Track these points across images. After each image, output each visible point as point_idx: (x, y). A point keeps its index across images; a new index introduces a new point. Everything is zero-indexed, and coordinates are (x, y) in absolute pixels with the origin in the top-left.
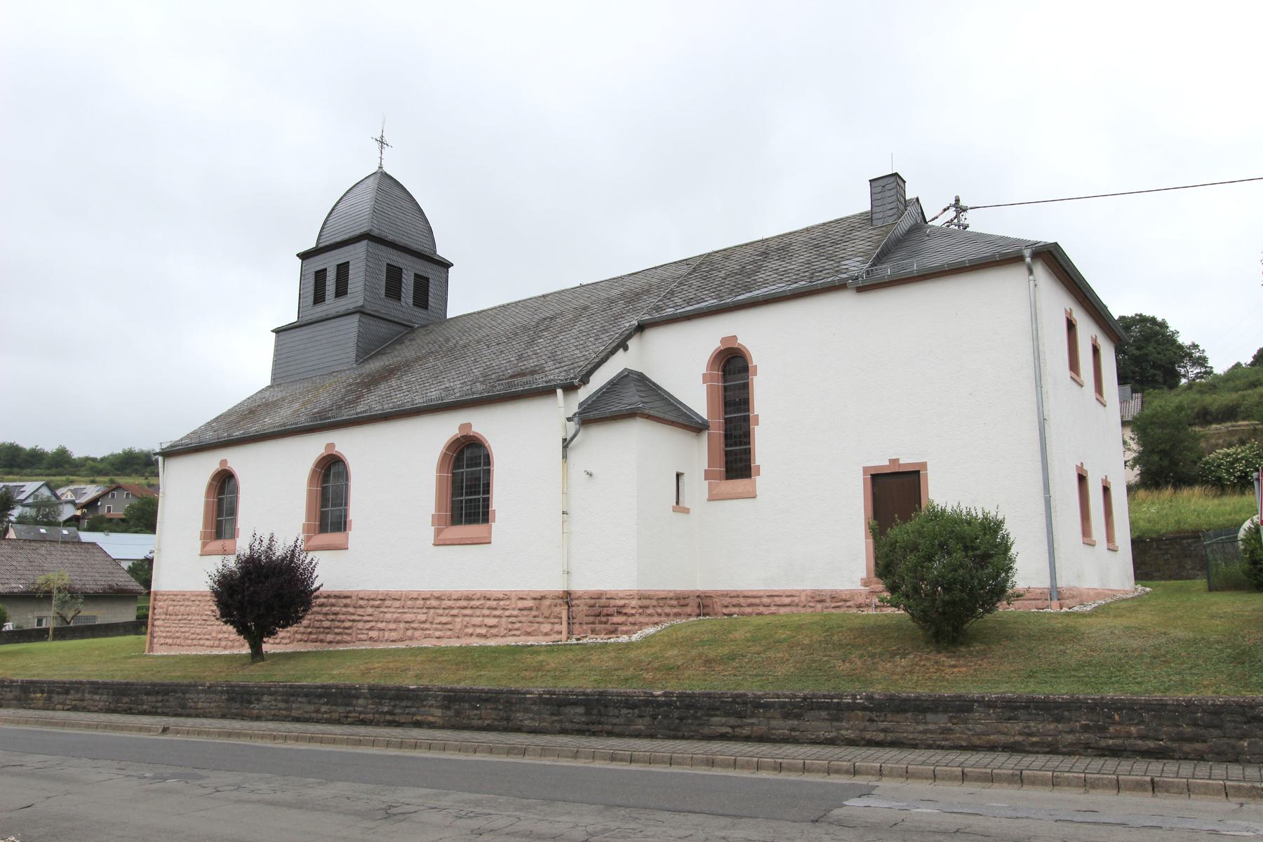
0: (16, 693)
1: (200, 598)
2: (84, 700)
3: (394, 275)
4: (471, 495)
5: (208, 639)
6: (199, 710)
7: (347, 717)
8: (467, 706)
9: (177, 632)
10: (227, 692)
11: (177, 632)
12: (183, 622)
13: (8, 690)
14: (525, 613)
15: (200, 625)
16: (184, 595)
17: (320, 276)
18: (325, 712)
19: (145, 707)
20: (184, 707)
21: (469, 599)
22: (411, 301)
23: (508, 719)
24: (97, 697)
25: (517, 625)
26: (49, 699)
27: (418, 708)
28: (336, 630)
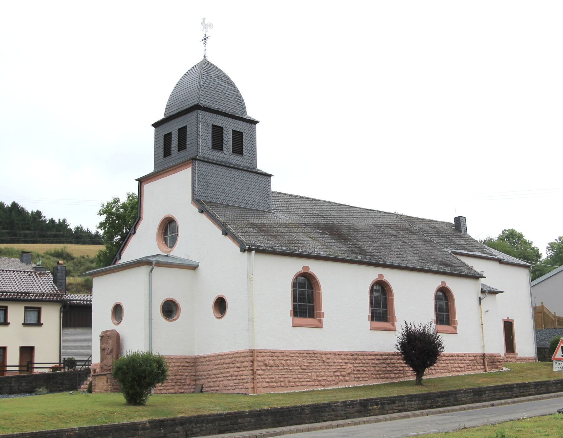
0: (357, 408)
2: (404, 406)
4: (301, 302)
6: (463, 402)
7: (512, 396)
8: (539, 387)
10: (473, 392)
11: (280, 378)
13: (351, 407)
14: (471, 362)
16: (283, 353)
17: (167, 137)
18: (507, 395)
19: (439, 404)
20: (456, 401)
21: (452, 356)
23: (548, 389)
24: (412, 403)
25: (470, 367)
26: (383, 408)
27: (529, 389)
28: (395, 372)
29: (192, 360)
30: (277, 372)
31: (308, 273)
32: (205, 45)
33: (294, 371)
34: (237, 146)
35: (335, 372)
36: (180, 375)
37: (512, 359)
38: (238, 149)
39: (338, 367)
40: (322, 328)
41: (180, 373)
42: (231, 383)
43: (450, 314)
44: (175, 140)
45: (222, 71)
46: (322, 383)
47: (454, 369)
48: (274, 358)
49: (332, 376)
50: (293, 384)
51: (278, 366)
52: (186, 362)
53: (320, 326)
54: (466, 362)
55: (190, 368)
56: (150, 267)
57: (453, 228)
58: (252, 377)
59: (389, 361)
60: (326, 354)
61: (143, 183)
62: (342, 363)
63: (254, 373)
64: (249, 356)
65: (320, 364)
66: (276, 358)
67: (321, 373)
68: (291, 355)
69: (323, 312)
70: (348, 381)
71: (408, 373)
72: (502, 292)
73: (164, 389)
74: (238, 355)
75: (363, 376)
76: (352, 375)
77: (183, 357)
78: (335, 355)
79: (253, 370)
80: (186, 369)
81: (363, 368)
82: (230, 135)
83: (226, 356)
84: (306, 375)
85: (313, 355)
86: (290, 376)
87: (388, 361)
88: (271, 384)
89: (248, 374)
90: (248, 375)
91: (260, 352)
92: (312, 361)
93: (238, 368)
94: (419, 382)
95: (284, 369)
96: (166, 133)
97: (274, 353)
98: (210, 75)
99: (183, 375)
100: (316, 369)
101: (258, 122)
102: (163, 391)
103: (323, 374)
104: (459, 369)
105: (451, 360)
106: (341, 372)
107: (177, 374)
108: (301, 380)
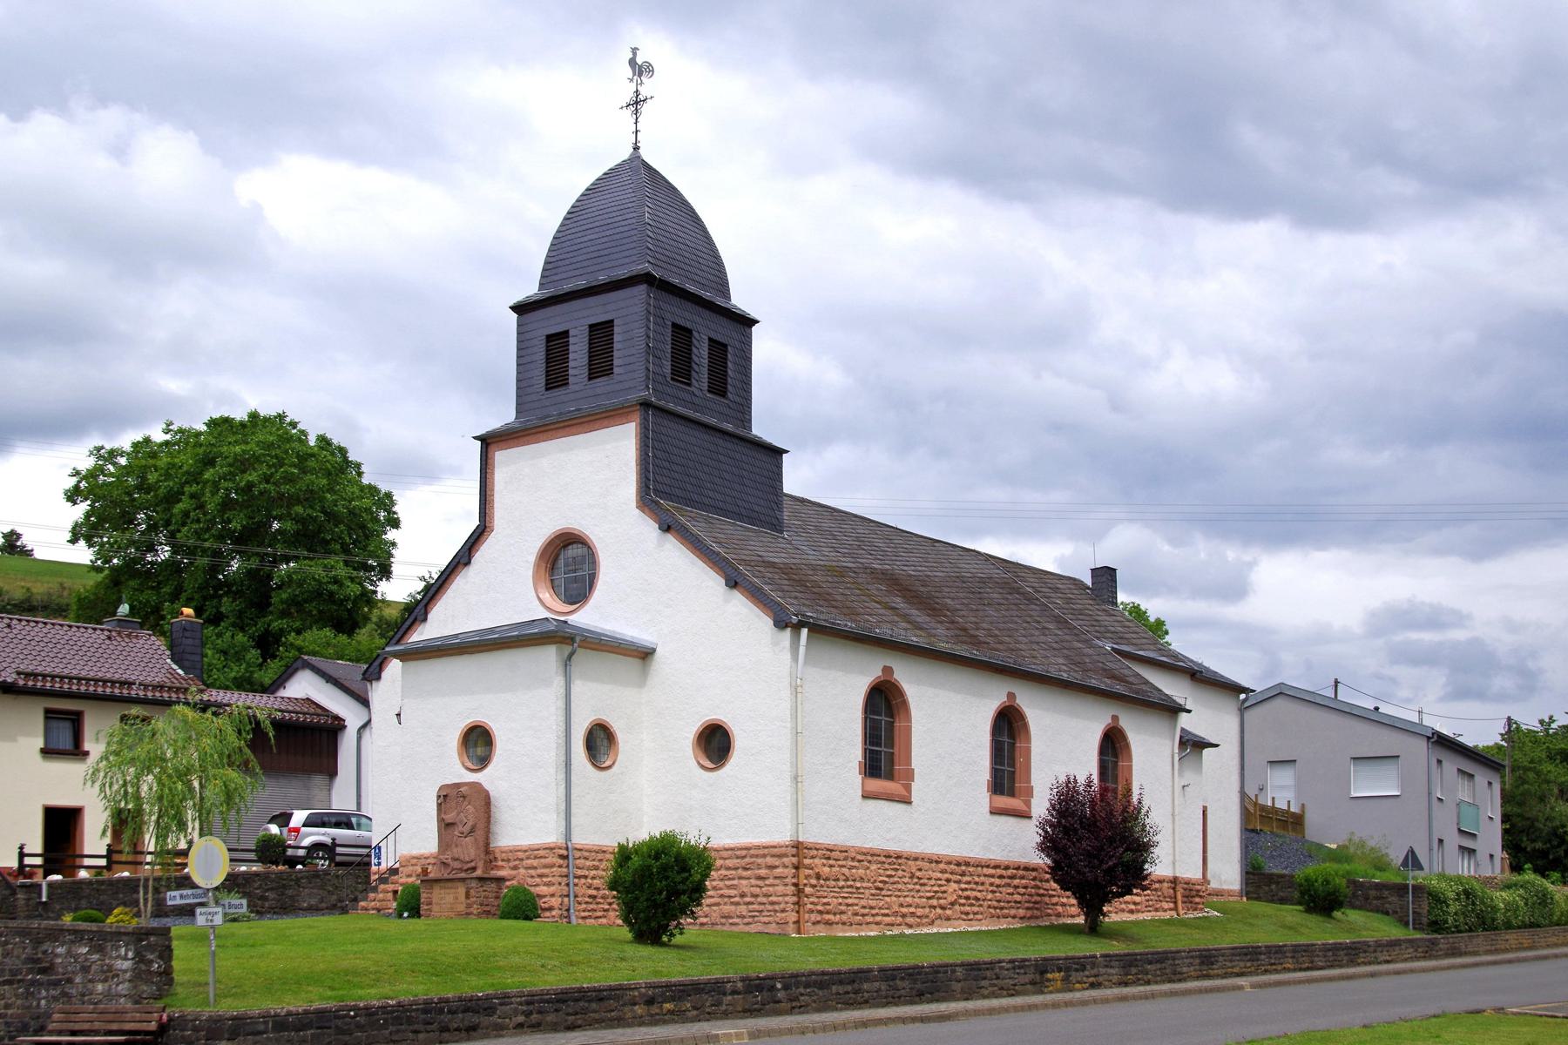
1: (869, 858)
2: (1098, 976)
3: (682, 335)
4: (873, 746)
5: (887, 915)
9: (840, 904)
11: (840, 904)
12: (846, 890)
13: (1022, 971)
15: (873, 895)
16: (846, 851)
17: (557, 343)
22: (705, 386)
32: (637, 118)
34: (602, 367)
40: (909, 803)
42: (743, 909)
44: (638, 356)
46: (910, 920)
49: (925, 907)
56: (567, 649)
58: (795, 899)
59: (1018, 881)
60: (916, 859)
61: (491, 448)
63: (799, 892)
64: (790, 855)
65: (906, 880)
67: (907, 899)
71: (1049, 909)
72: (1217, 746)
74: (761, 852)
75: (975, 909)
76: (957, 907)
78: (931, 861)
79: (796, 885)
82: (705, 352)
83: (730, 852)
86: (856, 901)
87: (1016, 882)
88: (827, 917)
90: (787, 895)
93: (760, 878)
94: (1093, 928)
96: (553, 332)
97: (831, 851)
98: (657, 198)
100: (899, 890)
101: (758, 322)
104: (1133, 907)
108: (874, 912)
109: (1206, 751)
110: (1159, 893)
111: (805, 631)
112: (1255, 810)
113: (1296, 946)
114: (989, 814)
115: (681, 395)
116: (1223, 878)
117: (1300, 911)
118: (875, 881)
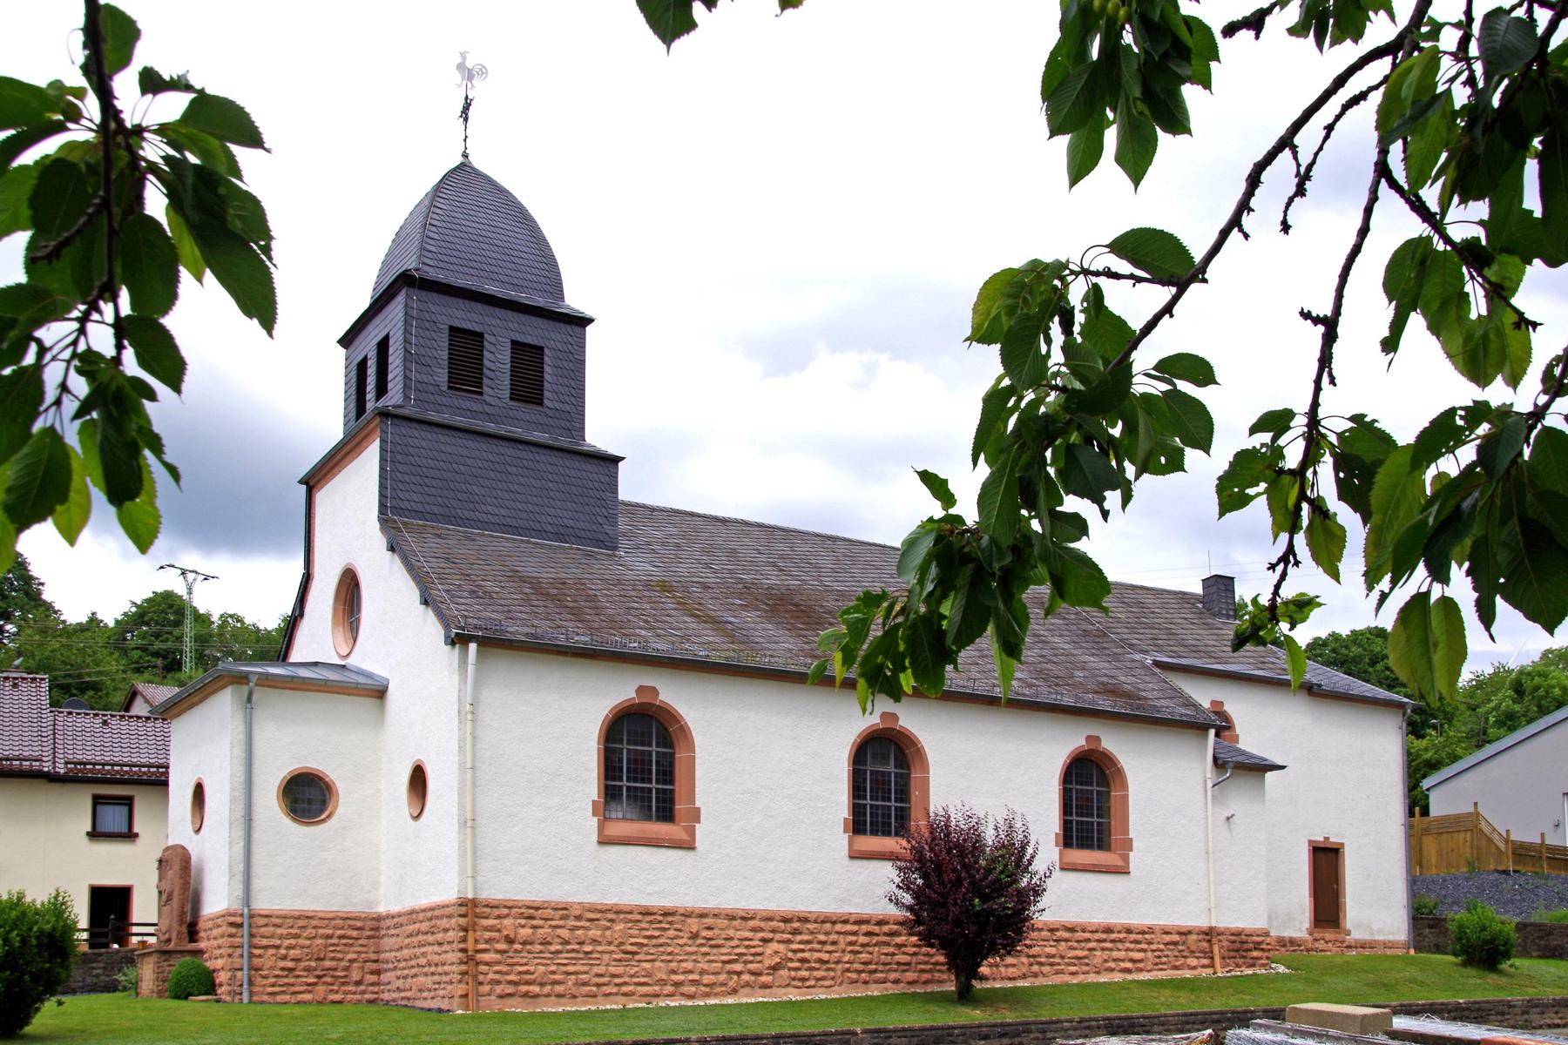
15: (615, 960)
21: (1108, 930)
22: (507, 394)
29: (369, 923)
30: (542, 958)
31: (654, 705)
33: (598, 956)
35: (729, 962)
36: (333, 959)
37: (1330, 945)
38: (528, 386)
39: (738, 951)
41: (333, 955)
43: (1113, 823)
45: (507, 192)
47: (1112, 965)
48: (535, 922)
50: (594, 989)
51: (550, 943)
52: (350, 926)
53: (687, 845)
54: (1153, 947)
55: (361, 942)
56: (245, 689)
57: (1197, 608)
62: (751, 940)
66: (541, 922)
67: (684, 965)
68: (591, 916)
69: (699, 809)
70: (770, 987)
72: (1282, 767)
73: (283, 992)
77: (341, 915)
80: (351, 945)
81: (817, 955)
82: (505, 355)
84: (636, 969)
85: (660, 918)
88: (524, 988)
89: (455, 960)
91: (491, 907)
92: (657, 933)
94: (965, 995)
95: (569, 951)
97: (537, 909)
99: (341, 960)
100: (670, 954)
102: (279, 998)
103: (689, 965)
104: (1129, 965)
105: (1105, 941)
106: (746, 962)
107: (322, 956)
109: (1269, 775)
110: (1180, 948)
111: (473, 647)
112: (1507, 849)
113: (1185, 1015)
114: (847, 859)
115: (474, 406)
116: (1375, 927)
117: (1457, 965)
118: (621, 944)
